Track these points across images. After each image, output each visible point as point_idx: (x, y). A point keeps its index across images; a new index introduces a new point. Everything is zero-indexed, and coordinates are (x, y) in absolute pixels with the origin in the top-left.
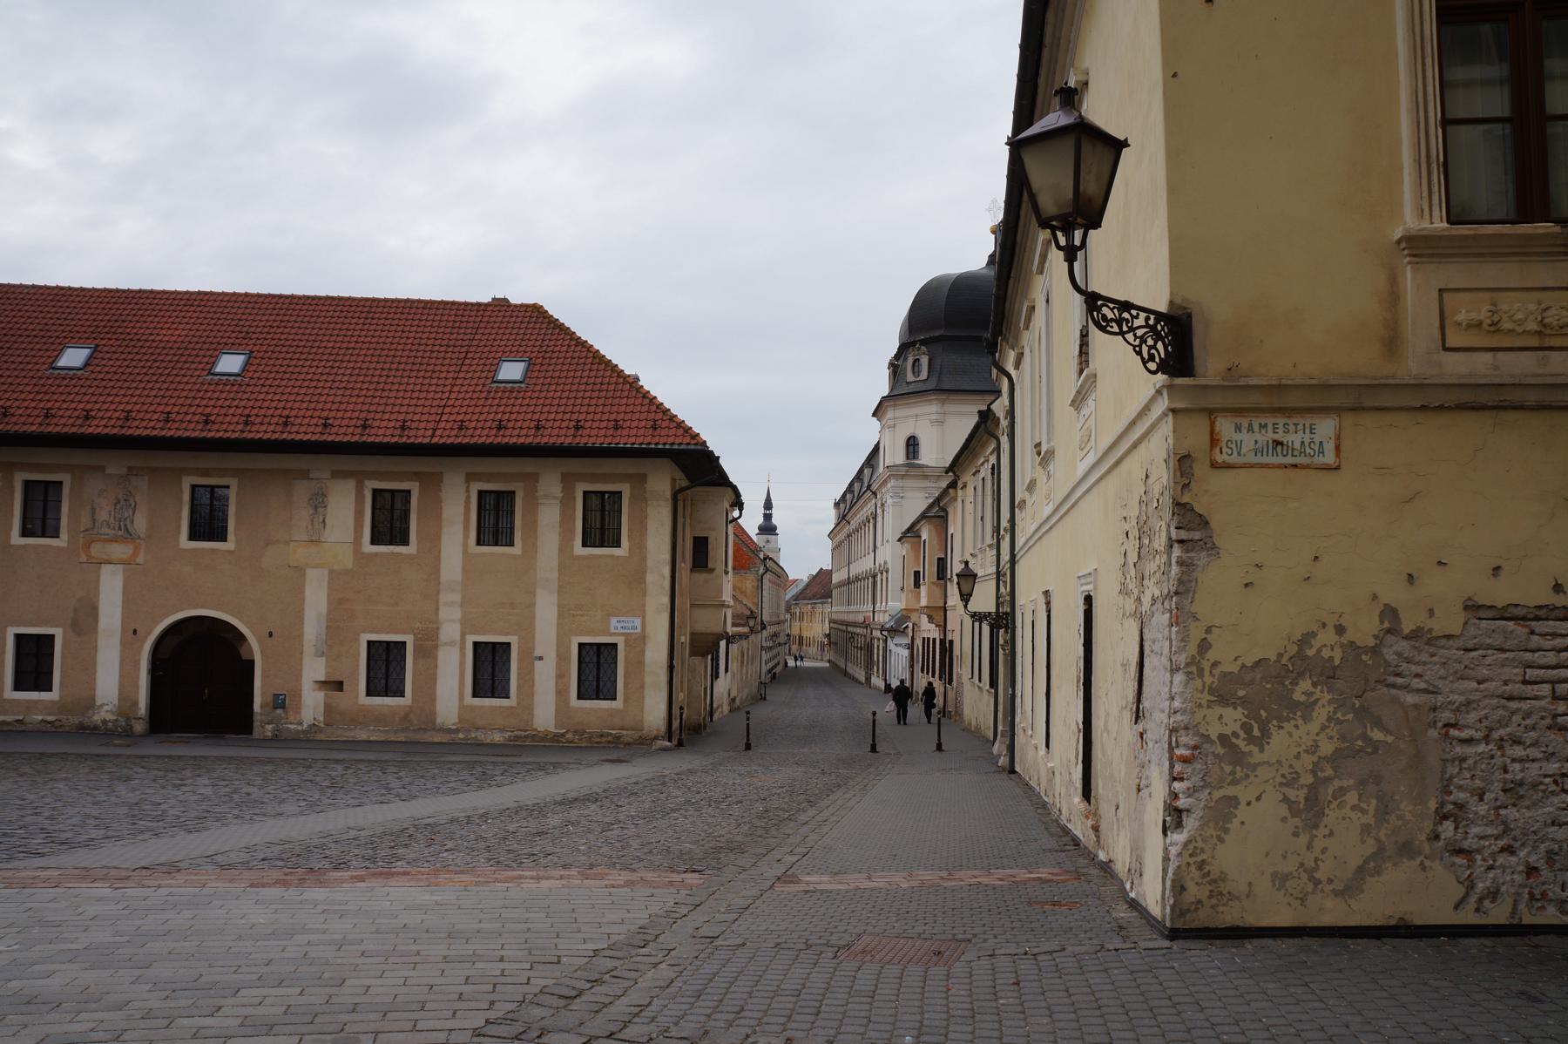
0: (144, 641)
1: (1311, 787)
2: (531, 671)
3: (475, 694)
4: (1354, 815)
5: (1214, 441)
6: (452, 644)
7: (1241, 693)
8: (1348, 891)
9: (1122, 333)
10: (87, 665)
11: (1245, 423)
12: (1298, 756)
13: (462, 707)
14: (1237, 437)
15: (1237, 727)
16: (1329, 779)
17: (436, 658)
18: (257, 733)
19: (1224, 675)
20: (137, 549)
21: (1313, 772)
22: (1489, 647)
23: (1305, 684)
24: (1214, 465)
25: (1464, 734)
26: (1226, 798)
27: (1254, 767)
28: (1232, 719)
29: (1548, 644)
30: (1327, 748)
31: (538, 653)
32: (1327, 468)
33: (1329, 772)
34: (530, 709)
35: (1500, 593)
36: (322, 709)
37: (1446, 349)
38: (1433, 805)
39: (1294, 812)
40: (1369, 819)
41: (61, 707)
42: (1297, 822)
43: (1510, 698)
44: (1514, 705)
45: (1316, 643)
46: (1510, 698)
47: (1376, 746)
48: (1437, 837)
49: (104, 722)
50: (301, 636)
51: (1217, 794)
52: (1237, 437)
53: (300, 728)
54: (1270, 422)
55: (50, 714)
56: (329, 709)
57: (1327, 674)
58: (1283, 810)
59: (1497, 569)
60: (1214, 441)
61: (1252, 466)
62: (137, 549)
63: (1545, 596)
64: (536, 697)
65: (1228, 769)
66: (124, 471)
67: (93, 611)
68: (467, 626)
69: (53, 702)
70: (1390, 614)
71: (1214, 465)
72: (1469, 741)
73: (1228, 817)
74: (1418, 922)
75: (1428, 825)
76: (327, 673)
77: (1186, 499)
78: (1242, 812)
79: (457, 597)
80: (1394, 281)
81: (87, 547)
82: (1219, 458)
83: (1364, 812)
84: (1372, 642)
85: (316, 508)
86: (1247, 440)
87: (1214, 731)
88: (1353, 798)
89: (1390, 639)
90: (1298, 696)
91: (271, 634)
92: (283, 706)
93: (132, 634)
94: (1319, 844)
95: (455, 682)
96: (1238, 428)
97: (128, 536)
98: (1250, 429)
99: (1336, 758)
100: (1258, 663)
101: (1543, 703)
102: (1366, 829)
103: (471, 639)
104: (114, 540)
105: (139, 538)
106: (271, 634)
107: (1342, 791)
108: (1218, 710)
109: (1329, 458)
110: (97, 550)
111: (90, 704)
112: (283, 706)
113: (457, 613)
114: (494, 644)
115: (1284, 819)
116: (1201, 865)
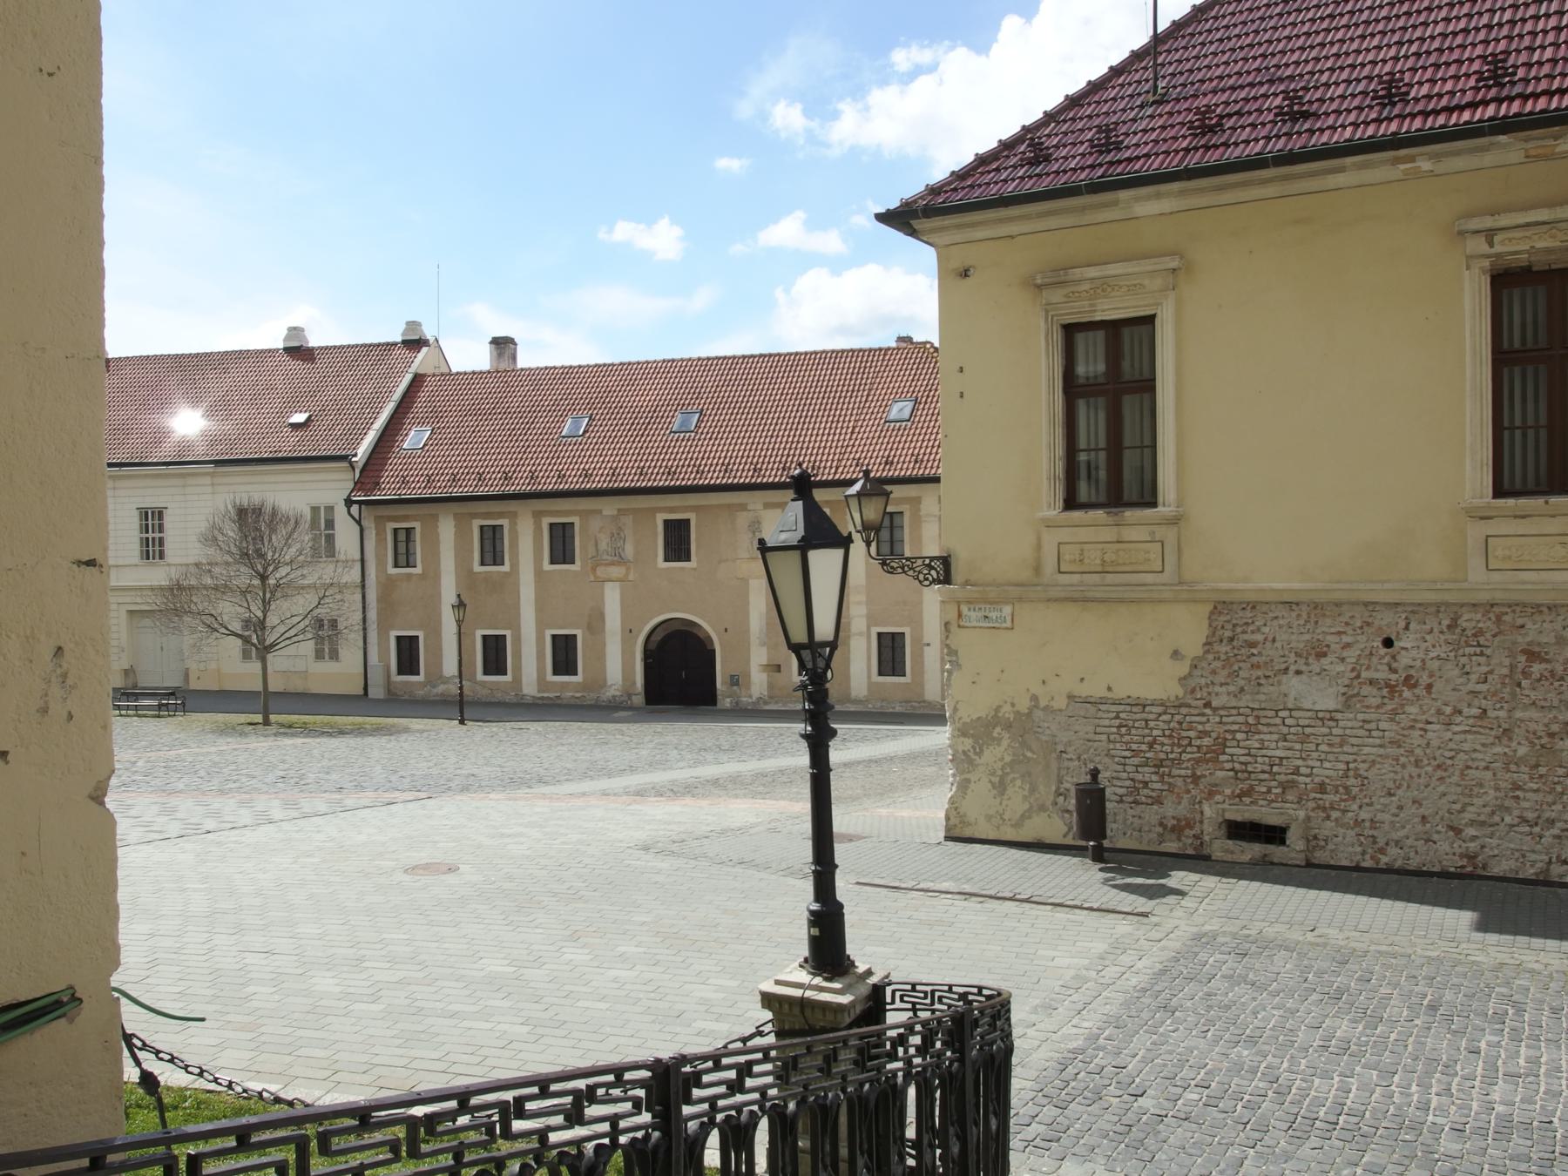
0: (637, 637)
1: (1001, 776)
2: (921, 655)
3: (880, 674)
4: (1020, 791)
5: (960, 615)
6: (860, 634)
7: (972, 732)
8: (1018, 825)
9: (904, 572)
10: (601, 657)
11: (972, 607)
12: (995, 762)
13: (870, 685)
14: (969, 614)
15: (969, 747)
16: (1008, 774)
17: (849, 645)
18: (719, 706)
19: (964, 724)
20: (628, 569)
21: (1002, 769)
22: (1079, 716)
23: (998, 729)
24: (959, 626)
25: (1068, 757)
26: (966, 779)
27: (977, 765)
28: (968, 743)
29: (1106, 716)
30: (1008, 759)
31: (926, 640)
32: (1007, 628)
33: (1008, 770)
34: (921, 685)
35: (1083, 690)
36: (766, 687)
37: (1060, 572)
38: (1054, 788)
39: (994, 787)
40: (1026, 793)
41: (584, 686)
42: (995, 792)
43: (1089, 741)
44: (1091, 743)
45: (1003, 710)
46: (1089, 741)
47: (1029, 759)
48: (1056, 804)
49: (614, 697)
50: (748, 631)
51: (963, 777)
52: (969, 614)
53: (750, 701)
54: (983, 607)
55: (578, 692)
56: (771, 686)
57: (1008, 726)
58: (989, 786)
59: (1082, 679)
60: (960, 615)
61: (975, 627)
62: (628, 569)
63: (1104, 693)
64: (926, 676)
65: (966, 766)
66: (615, 512)
67: (601, 617)
68: (871, 620)
69: (579, 683)
70: (1034, 698)
71: (959, 626)
72: (1071, 759)
73: (966, 788)
74: (1047, 842)
75: (1052, 798)
76: (768, 660)
77: (948, 642)
78: (972, 786)
79: (863, 598)
80: (1039, 539)
81: (594, 570)
82: (961, 624)
83: (1024, 789)
84: (1026, 711)
85: (754, 532)
86: (973, 614)
87: (960, 748)
88: (1018, 782)
89: (1035, 710)
90: (995, 735)
91: (726, 630)
92: (737, 684)
93: (629, 632)
94: (1004, 803)
95: (864, 665)
96: (969, 609)
97: (621, 560)
98: (974, 610)
99: (1012, 764)
100: (979, 718)
101: (1103, 744)
102: (1025, 798)
103: (875, 630)
104: (612, 564)
105: (629, 561)
106: (726, 630)
107: (1014, 779)
108: (962, 739)
109: (1008, 624)
110: (601, 571)
111: (603, 684)
112: (737, 684)
113: (863, 610)
114: (893, 634)
115: (990, 791)
116: (956, 809)
